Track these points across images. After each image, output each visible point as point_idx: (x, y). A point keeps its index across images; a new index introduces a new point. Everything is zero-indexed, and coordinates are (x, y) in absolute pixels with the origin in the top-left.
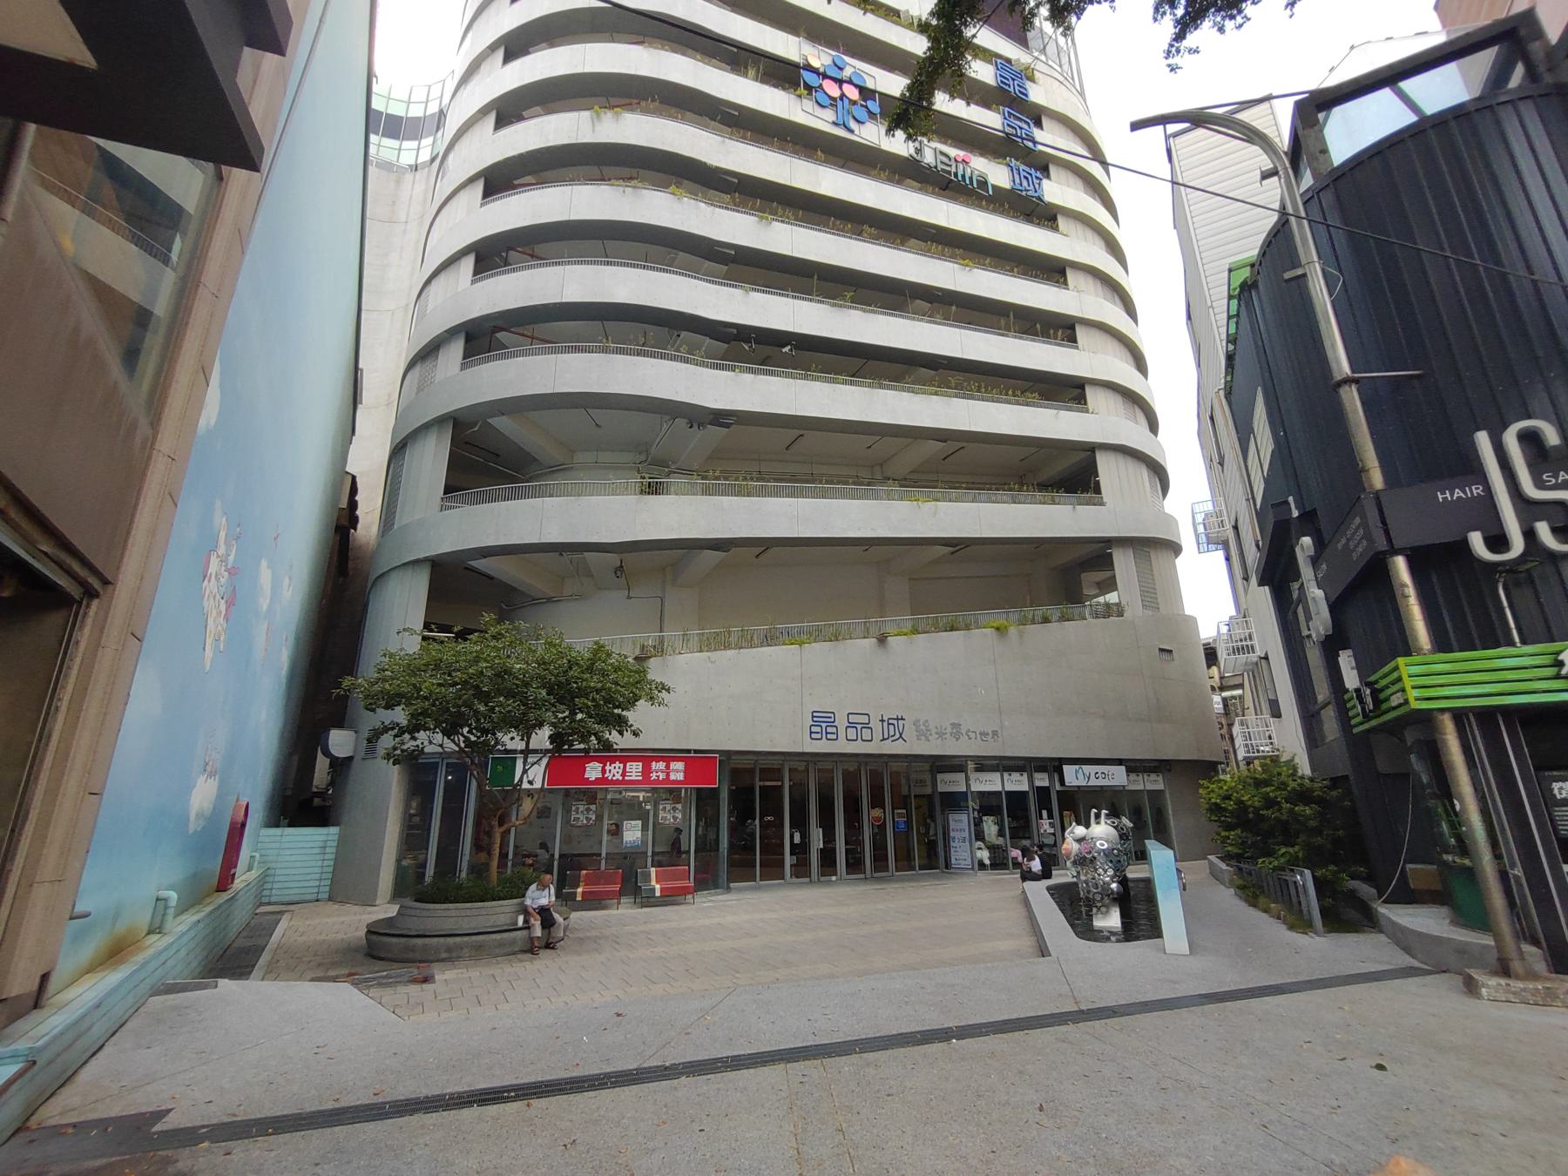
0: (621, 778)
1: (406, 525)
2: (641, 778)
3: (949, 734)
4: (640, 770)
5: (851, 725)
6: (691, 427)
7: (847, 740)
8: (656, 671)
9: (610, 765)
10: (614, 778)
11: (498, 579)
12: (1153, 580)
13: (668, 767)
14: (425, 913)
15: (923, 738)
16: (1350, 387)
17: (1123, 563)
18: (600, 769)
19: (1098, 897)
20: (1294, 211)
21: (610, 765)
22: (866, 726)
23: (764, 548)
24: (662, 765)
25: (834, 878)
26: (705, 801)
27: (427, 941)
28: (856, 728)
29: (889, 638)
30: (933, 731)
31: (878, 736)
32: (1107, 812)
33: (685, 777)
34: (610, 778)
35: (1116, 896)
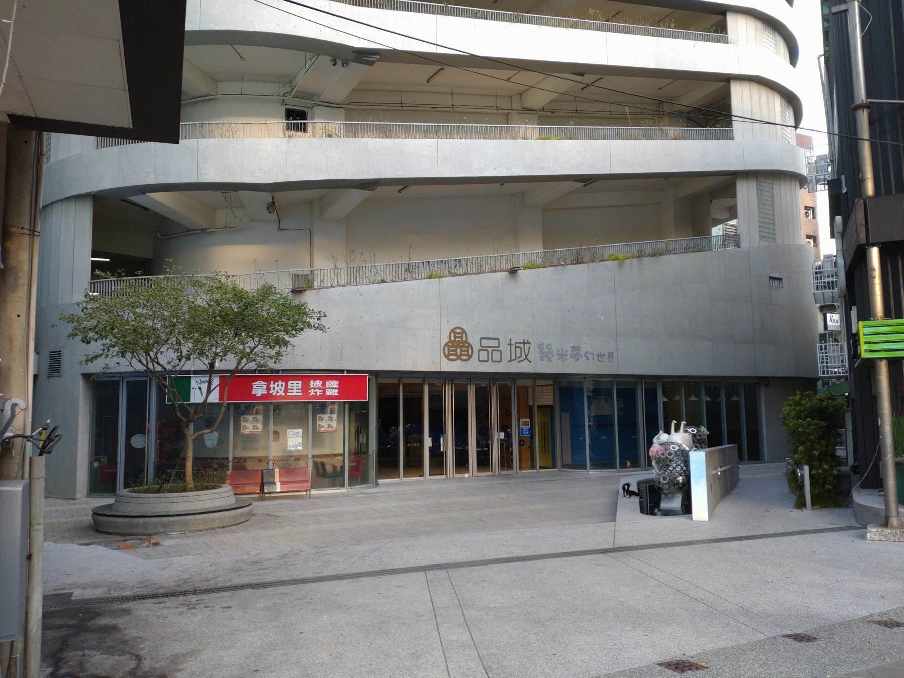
0: (283, 394)
1: (62, 160)
2: (301, 394)
3: (569, 356)
4: (300, 387)
6: (334, 65)
7: (479, 361)
8: (311, 300)
9: (274, 384)
10: (278, 394)
11: (151, 210)
12: (773, 211)
13: (324, 384)
14: (140, 500)
15: (546, 359)
16: (863, 111)
17: (745, 192)
18: (265, 386)
19: (667, 486)
21: (274, 384)
22: (496, 349)
23: (402, 187)
24: (319, 383)
25: (466, 475)
26: (358, 413)
27: (147, 520)
28: (488, 351)
29: (519, 271)
30: (555, 353)
32: (685, 423)
33: (339, 392)
34: (274, 394)
35: (681, 486)
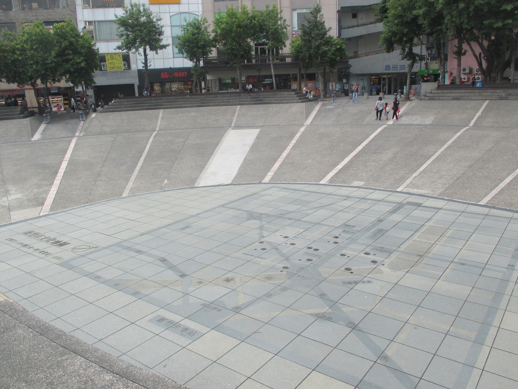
5: (394, 67)
20: (513, 218)
22: (397, 67)
31: (399, 69)
